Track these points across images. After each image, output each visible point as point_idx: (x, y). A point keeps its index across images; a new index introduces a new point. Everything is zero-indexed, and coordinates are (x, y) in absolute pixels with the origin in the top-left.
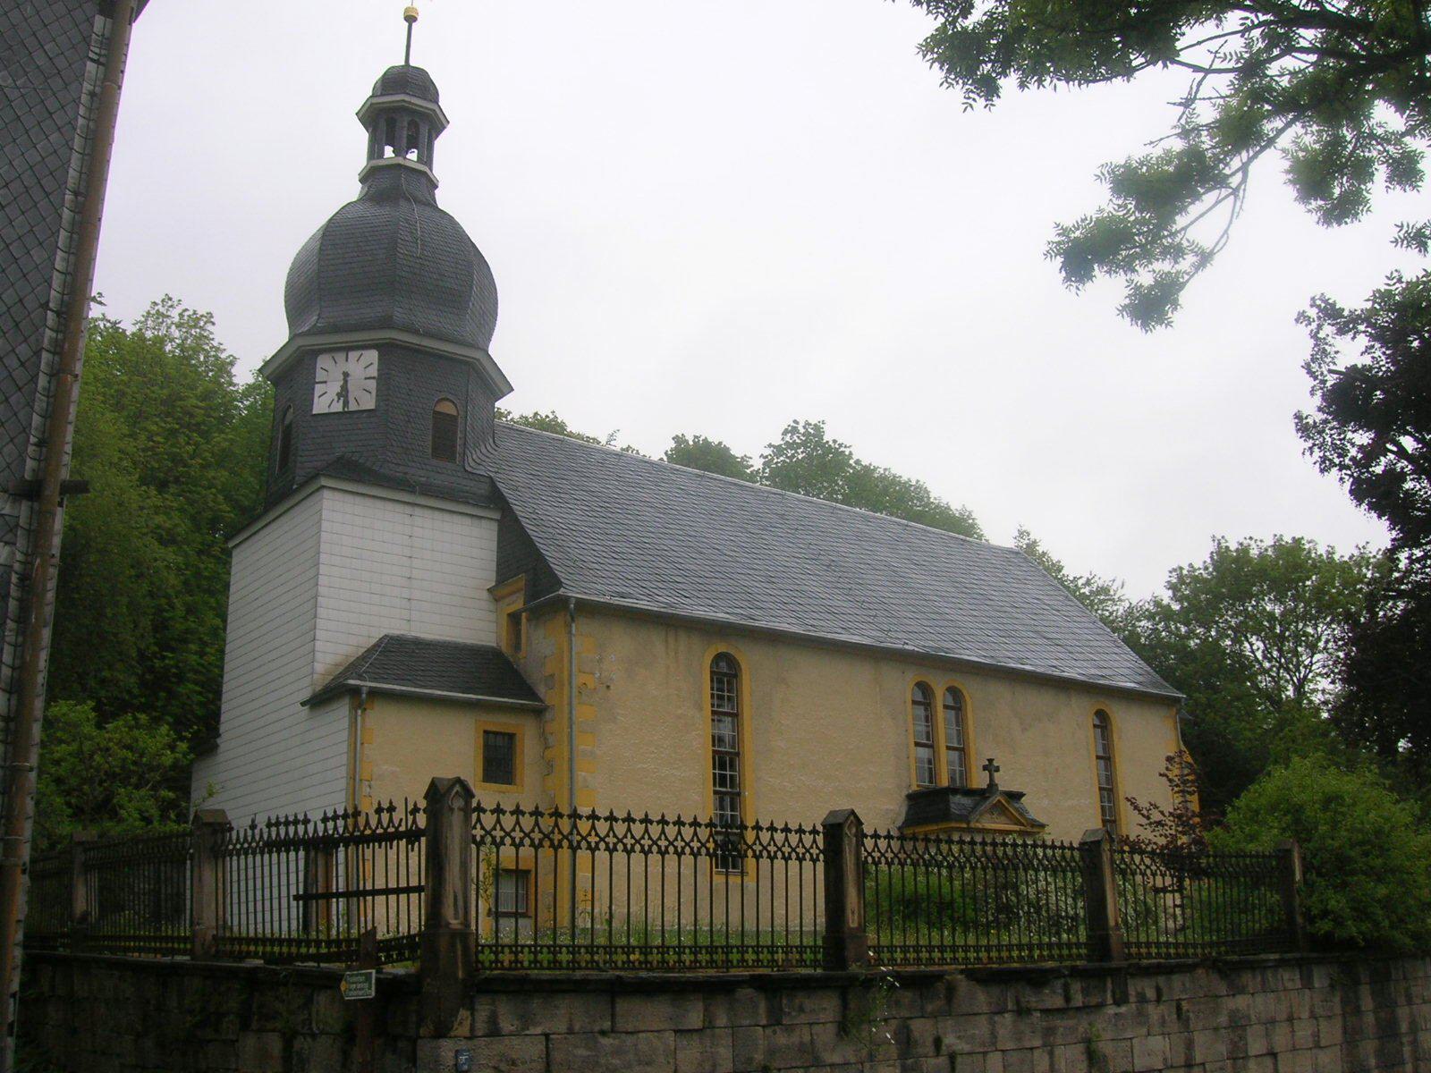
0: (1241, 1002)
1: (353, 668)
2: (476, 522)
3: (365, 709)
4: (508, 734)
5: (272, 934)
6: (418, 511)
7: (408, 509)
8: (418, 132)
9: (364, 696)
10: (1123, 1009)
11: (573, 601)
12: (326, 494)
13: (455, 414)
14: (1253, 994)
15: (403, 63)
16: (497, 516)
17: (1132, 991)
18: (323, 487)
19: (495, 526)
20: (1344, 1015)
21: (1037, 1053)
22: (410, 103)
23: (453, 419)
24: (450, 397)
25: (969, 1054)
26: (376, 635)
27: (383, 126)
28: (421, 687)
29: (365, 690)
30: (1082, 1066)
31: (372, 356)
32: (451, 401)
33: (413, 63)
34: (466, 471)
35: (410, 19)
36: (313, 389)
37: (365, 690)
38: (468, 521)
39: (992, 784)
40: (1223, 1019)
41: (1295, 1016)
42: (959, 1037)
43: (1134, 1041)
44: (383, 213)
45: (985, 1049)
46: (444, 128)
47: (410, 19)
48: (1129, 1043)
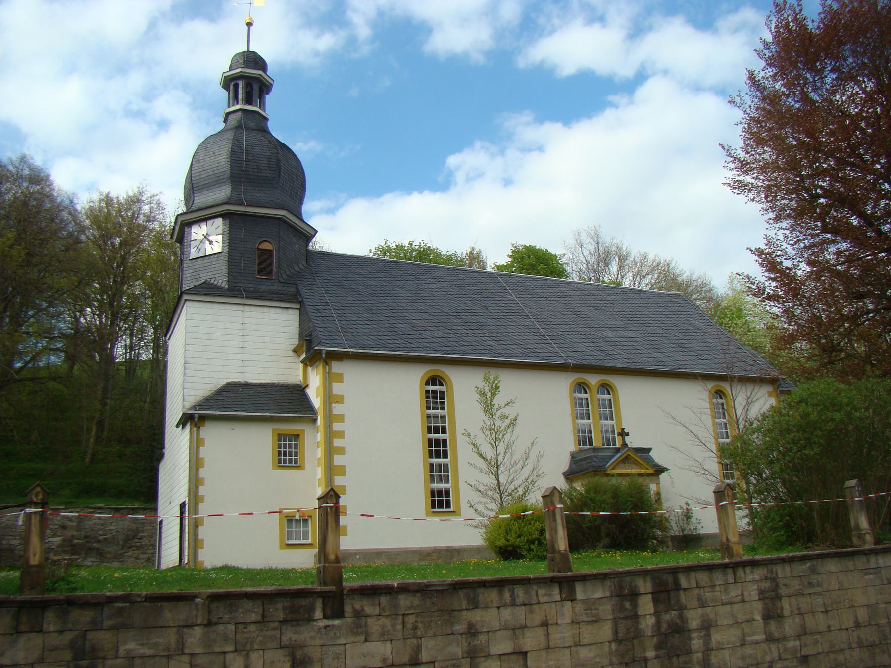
0: (476, 616)
1: (201, 405)
2: (285, 311)
3: (199, 427)
4: (295, 435)
5: (747, 516)
6: (247, 308)
7: (241, 308)
8: (252, 89)
9: (196, 419)
10: (337, 622)
11: (324, 352)
12: (188, 304)
13: (272, 249)
14: (498, 608)
15: (245, 50)
16: (298, 306)
17: (348, 609)
18: (186, 300)
19: (297, 312)
20: (615, 621)
21: (229, 657)
22: (244, 72)
23: (270, 252)
25: (154, 656)
26: (224, 382)
28: (236, 411)
29: (196, 416)
30: (242, 667)
31: (219, 221)
32: (268, 241)
33: (251, 50)
34: (280, 282)
35: (249, 25)
36: (190, 245)
37: (196, 416)
39: (625, 445)
40: (460, 628)
41: (550, 622)
42: (142, 645)
43: (347, 646)
45: (170, 653)
46: (271, 85)
47: (249, 25)
48: (342, 648)
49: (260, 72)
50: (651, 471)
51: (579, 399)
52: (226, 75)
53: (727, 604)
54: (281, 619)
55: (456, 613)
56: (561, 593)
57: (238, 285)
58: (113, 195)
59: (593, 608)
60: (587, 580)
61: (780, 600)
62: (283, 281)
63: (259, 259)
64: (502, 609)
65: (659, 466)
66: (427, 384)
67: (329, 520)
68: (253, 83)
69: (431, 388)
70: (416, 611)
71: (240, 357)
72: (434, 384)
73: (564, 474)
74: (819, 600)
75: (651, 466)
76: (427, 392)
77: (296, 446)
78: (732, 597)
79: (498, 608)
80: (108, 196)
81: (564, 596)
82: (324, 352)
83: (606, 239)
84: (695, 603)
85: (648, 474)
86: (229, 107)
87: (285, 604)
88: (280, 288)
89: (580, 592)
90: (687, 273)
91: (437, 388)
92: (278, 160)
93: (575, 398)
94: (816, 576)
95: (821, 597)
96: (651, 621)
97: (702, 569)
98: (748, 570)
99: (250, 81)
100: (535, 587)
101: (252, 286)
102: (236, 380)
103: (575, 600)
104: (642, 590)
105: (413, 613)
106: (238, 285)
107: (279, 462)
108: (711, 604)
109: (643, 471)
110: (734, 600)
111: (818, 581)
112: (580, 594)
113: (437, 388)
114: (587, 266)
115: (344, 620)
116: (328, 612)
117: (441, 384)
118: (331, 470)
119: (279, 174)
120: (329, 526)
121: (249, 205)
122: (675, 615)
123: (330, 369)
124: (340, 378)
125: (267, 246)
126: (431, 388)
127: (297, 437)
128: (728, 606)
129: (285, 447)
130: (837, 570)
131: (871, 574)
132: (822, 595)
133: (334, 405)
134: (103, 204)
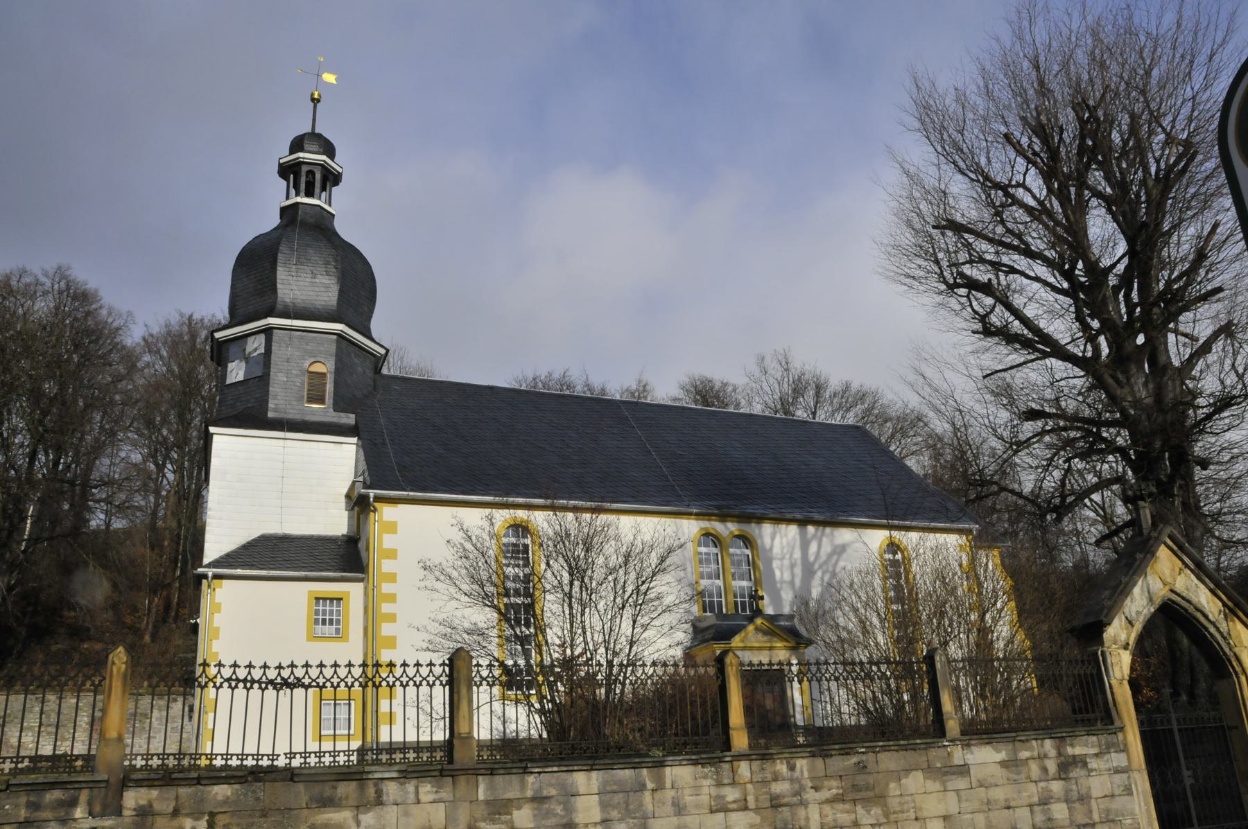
8: (314, 178)
23: (323, 375)
26: (255, 534)
35: (315, 101)
47: (315, 101)
49: (324, 158)
51: (706, 554)
52: (282, 161)
53: (718, 811)
54: (22, 819)
55: (295, 812)
58: (196, 317)
59: (501, 811)
61: (806, 808)
63: (310, 384)
64: (362, 809)
67: (114, 684)
70: (231, 809)
79: (357, 807)
80: (190, 317)
83: (797, 365)
84: (669, 809)
86: (287, 198)
87: (31, 799)
90: (900, 404)
93: (700, 553)
94: (863, 777)
97: (102, 719)
100: (414, 782)
104: (582, 790)
105: (225, 812)
108: (693, 812)
110: (731, 806)
111: (868, 784)
115: (120, 820)
116: (97, 808)
118: (370, 632)
120: (113, 693)
122: (635, 825)
128: (721, 815)
129: (324, 612)
130: (899, 768)
133: (383, 561)
134: (186, 329)
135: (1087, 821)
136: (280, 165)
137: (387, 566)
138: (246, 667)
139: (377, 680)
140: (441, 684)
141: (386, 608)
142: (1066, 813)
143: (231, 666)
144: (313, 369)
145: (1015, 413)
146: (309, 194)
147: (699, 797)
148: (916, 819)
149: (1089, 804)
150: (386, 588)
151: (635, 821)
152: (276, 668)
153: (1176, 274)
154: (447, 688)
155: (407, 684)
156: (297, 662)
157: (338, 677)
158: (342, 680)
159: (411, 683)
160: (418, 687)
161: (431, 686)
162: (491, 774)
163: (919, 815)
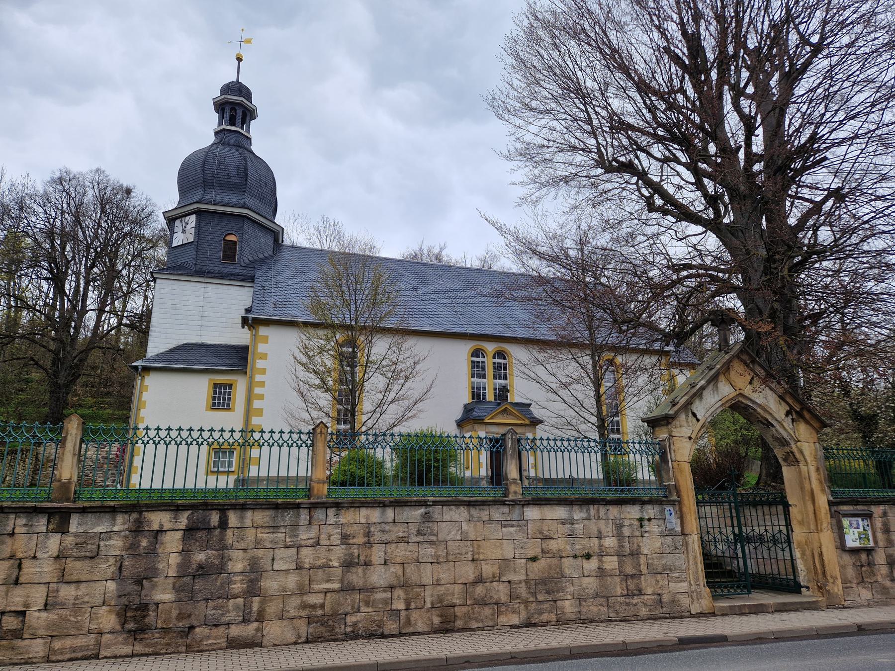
2: (242, 288)
7: (203, 285)
23: (235, 242)
24: (234, 233)
27: (227, 115)
29: (140, 367)
35: (239, 60)
37: (140, 367)
38: (237, 288)
44: (226, 151)
47: (239, 60)
50: (527, 422)
52: (215, 101)
56: (49, 522)
57: (205, 267)
60: (117, 512)
62: (244, 265)
63: (224, 247)
65: (535, 418)
66: (472, 356)
68: (237, 108)
69: (475, 359)
71: (199, 323)
72: (478, 356)
73: (456, 421)
74: (431, 550)
75: (528, 418)
76: (472, 362)
77: (230, 393)
78: (301, 539)
81: (51, 527)
82: (250, 319)
85: (525, 425)
88: (241, 271)
89: (75, 524)
91: (480, 359)
92: (246, 170)
95: (434, 547)
96: (174, 559)
98: (331, 512)
99: (234, 106)
100: (12, 516)
101: (216, 268)
102: (193, 341)
103: (68, 532)
106: (205, 267)
107: (214, 404)
109: (523, 422)
112: (73, 528)
113: (480, 359)
114: (865, 293)
117: (504, 358)
118: (249, 412)
119: (246, 180)
121: (215, 204)
123: (257, 332)
124: (265, 340)
125: (232, 238)
126: (475, 359)
127: (230, 386)
131: (513, 526)
132: (435, 544)
135: (635, 572)
136: (214, 103)
137: (260, 364)
138: (229, 431)
139: (262, 441)
140: (307, 446)
141: (257, 390)
142: (616, 565)
143: (229, 431)
144: (228, 238)
145: (836, 290)
146: (233, 124)
147: (275, 535)
148: (473, 560)
149: (638, 559)
150: (258, 378)
151: (213, 552)
152: (219, 431)
153: (675, 16)
154: (489, 452)
155: (273, 445)
156: (205, 428)
157: (148, 437)
158: (194, 440)
159: (276, 444)
160: (199, 446)
161: (299, 447)
162: (242, 509)
163: (476, 556)
